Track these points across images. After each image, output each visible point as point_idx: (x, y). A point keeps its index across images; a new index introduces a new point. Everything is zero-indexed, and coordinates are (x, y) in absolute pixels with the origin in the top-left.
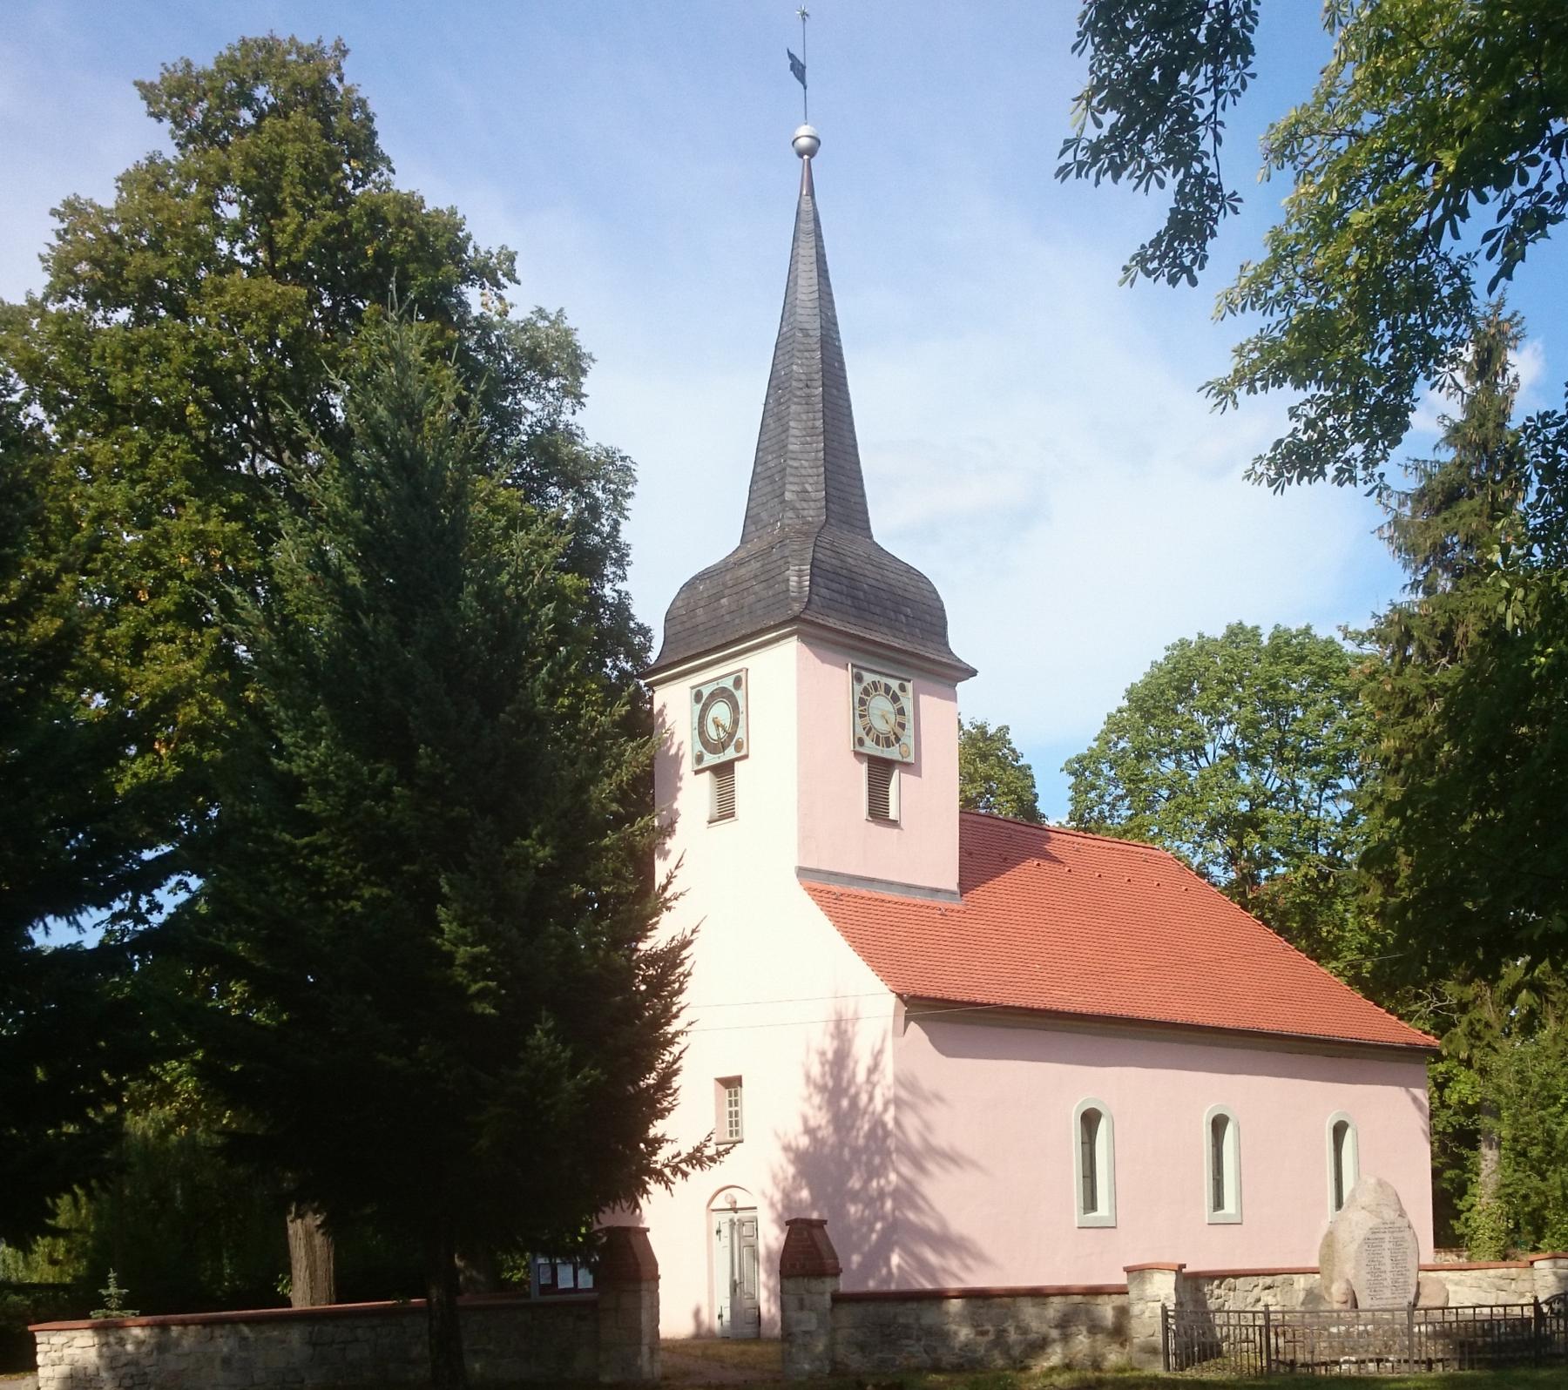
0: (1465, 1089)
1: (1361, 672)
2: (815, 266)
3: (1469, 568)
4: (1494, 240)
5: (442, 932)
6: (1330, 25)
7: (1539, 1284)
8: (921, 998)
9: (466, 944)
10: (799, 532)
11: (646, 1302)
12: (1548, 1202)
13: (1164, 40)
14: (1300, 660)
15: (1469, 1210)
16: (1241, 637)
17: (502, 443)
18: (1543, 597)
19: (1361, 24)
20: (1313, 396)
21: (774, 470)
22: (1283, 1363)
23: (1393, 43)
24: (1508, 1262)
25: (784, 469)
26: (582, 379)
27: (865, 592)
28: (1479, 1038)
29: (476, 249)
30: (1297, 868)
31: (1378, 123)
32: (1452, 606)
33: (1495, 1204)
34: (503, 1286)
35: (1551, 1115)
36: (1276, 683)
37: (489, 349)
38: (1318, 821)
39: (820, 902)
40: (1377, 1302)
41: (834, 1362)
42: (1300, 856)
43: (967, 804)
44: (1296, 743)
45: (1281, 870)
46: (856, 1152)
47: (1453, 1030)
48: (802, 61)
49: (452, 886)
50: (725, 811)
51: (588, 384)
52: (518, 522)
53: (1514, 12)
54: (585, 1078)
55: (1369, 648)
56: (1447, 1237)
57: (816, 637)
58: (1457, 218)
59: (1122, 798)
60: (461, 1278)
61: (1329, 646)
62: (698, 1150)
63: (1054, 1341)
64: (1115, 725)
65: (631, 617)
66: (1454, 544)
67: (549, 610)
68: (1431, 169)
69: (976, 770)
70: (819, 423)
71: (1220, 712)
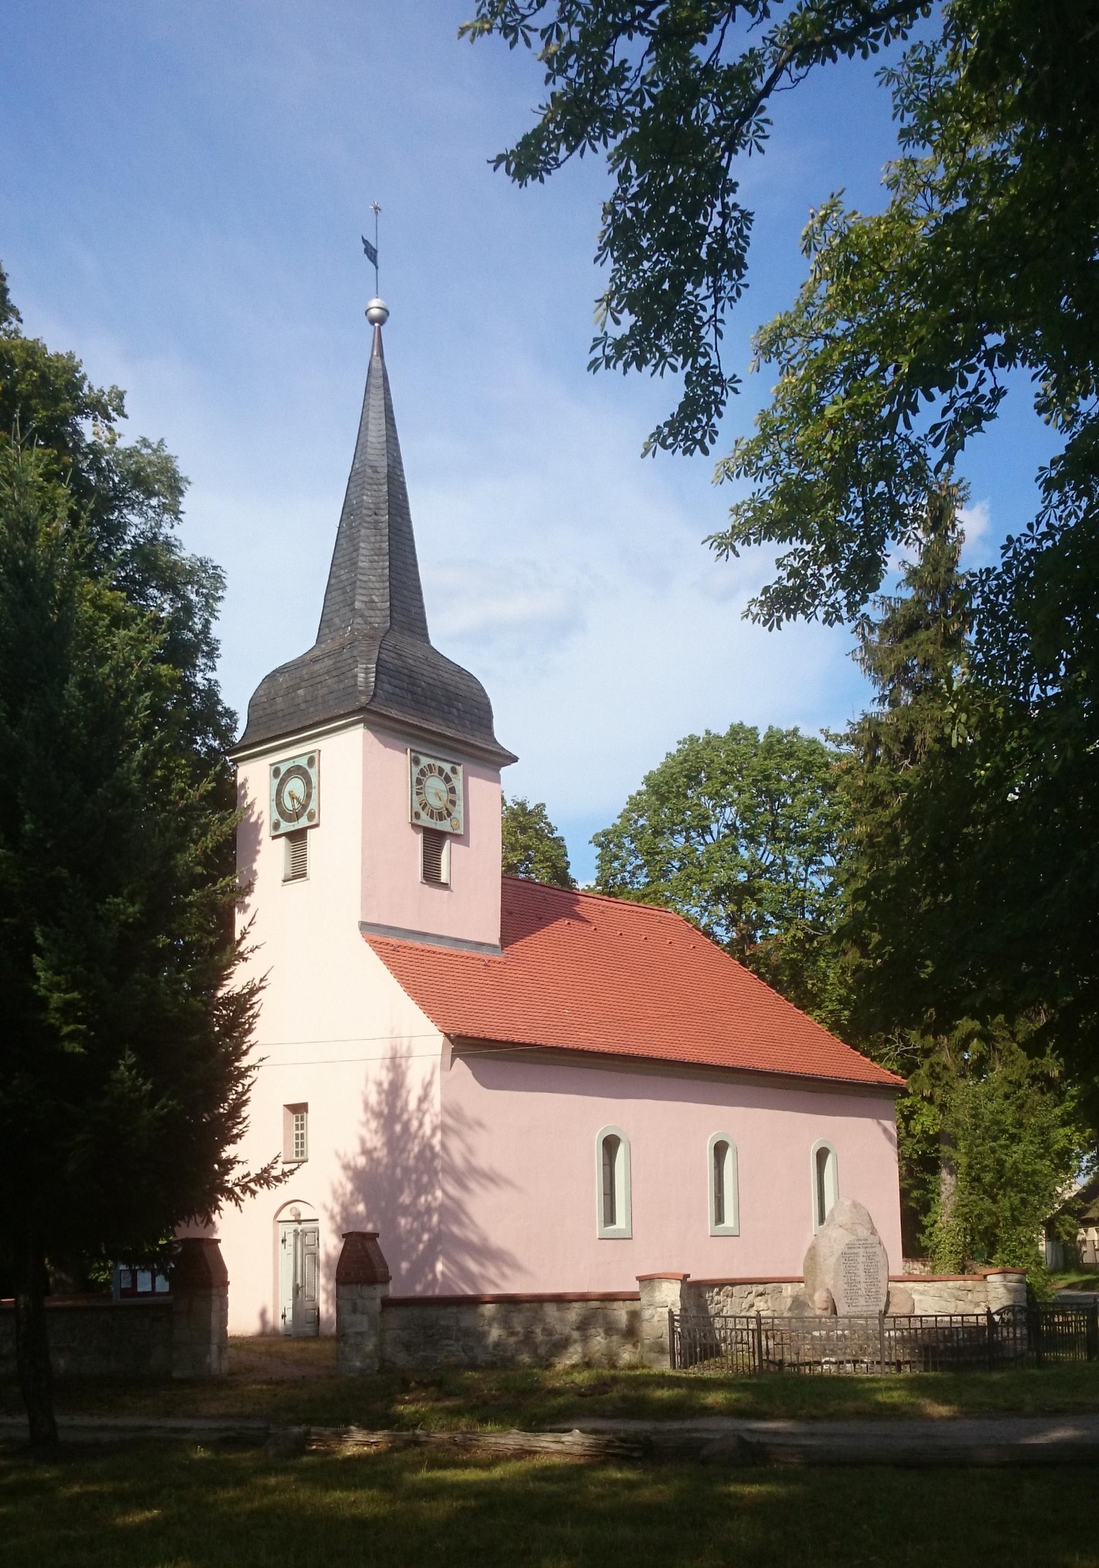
0: (927, 1121)
1: (839, 767)
2: (383, 415)
3: (926, 686)
4: (938, 432)
5: (38, 978)
6: (807, 250)
7: (992, 1295)
8: (466, 1038)
9: (60, 991)
10: (365, 635)
11: (216, 1306)
12: (999, 1222)
13: (672, 257)
14: (790, 756)
15: (932, 1225)
16: (742, 735)
17: (108, 550)
18: (982, 721)
19: (832, 250)
20: (796, 550)
21: (346, 583)
22: (773, 1362)
23: (858, 266)
24: (966, 1276)
26: (181, 499)
27: (423, 689)
28: (938, 1078)
29: (90, 388)
30: (787, 930)
31: (848, 329)
32: (913, 717)
33: (953, 1222)
34: (89, 1287)
35: (1001, 1146)
36: (770, 775)
37: (100, 471)
38: (805, 891)
39: (379, 952)
40: (854, 1309)
41: (383, 1360)
42: (790, 920)
43: (509, 870)
44: (786, 825)
45: (774, 931)
46: (406, 1171)
47: (917, 1071)
48: (374, 246)
49: (46, 937)
50: (297, 872)
51: (186, 503)
52: (120, 620)
53: (955, 249)
54: (162, 1108)
55: (845, 748)
56: (913, 1249)
57: (379, 725)
58: (909, 412)
59: (640, 867)
60: (51, 1280)
61: (813, 747)
62: (265, 1171)
63: (575, 1341)
64: (635, 805)
65: (219, 702)
66: (914, 666)
67: (146, 698)
68: (891, 369)
69: (517, 840)
70: (385, 545)
71: (722, 797)
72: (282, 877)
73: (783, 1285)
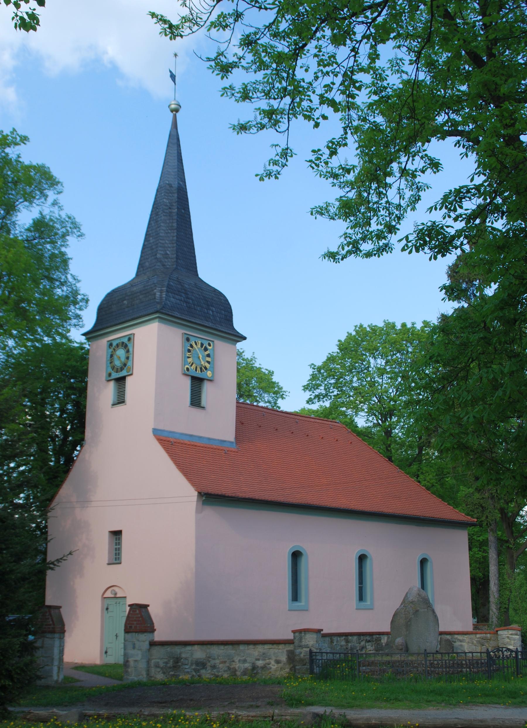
2: (176, 158)
25: (157, 244)
48: (174, 73)
50: (120, 400)
70: (175, 225)
73: (382, 636)
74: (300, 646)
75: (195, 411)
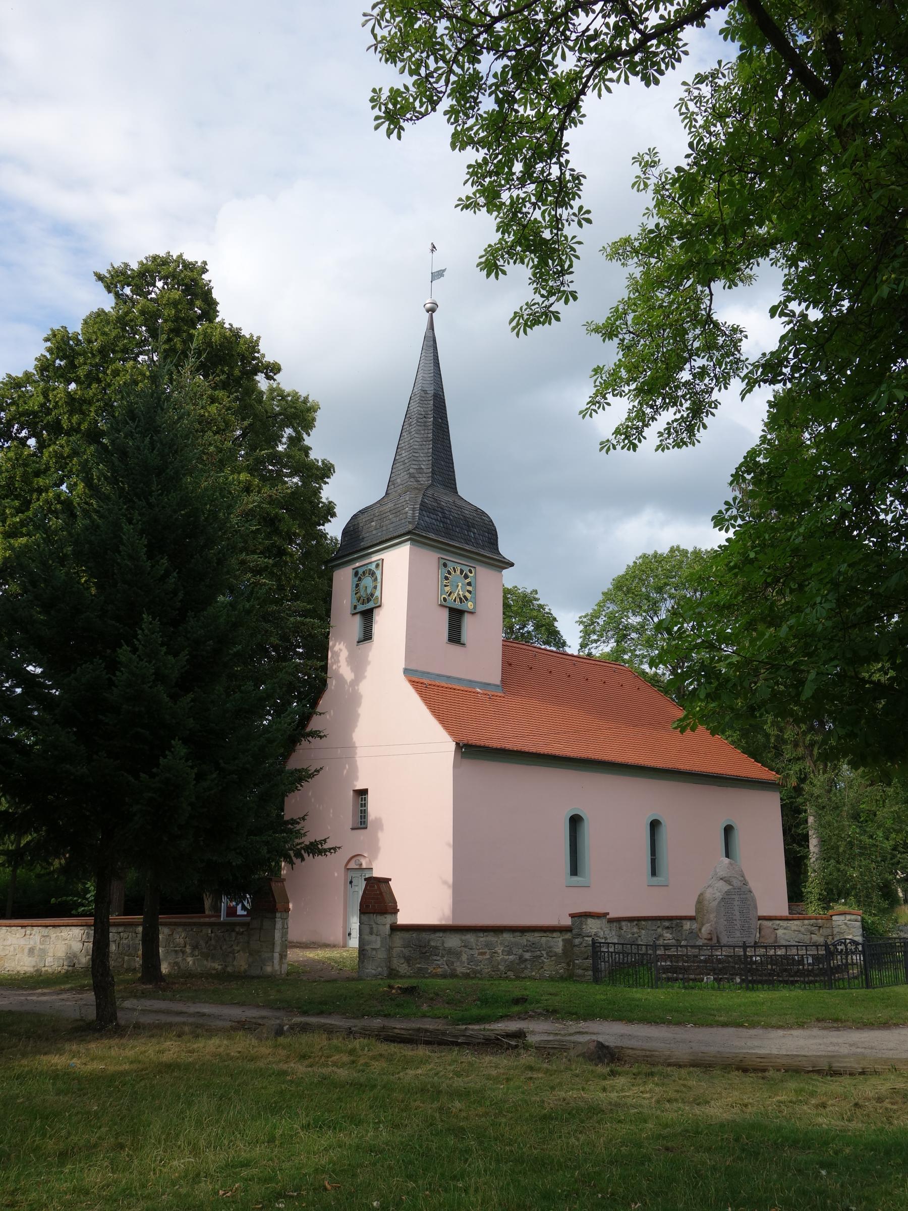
40: (730, 940)
70: (430, 435)
72: (357, 639)
73: (684, 922)
74: (579, 935)
75: (454, 648)
